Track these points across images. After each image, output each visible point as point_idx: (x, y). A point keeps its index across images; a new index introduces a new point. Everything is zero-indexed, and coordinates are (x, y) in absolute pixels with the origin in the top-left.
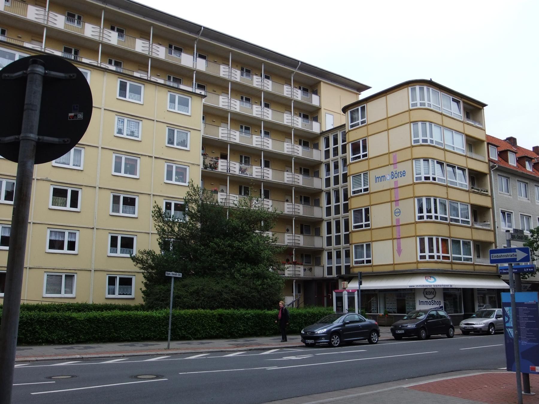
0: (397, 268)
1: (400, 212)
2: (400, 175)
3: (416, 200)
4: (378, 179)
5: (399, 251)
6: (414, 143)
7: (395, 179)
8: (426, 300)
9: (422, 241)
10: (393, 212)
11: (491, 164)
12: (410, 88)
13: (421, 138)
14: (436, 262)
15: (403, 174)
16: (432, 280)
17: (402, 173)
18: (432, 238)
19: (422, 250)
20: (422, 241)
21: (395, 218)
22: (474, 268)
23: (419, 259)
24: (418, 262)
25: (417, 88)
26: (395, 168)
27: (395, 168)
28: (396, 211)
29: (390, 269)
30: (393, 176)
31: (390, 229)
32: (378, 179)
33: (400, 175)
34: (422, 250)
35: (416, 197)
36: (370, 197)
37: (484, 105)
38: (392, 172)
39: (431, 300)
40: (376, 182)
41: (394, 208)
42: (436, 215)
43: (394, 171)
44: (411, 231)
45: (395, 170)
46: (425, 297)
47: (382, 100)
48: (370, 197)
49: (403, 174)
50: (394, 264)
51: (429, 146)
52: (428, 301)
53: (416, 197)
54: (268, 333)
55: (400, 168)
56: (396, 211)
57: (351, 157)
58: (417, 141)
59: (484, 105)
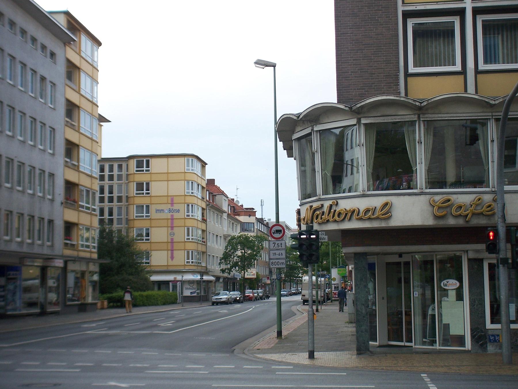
0: (171, 269)
1: (174, 234)
2: (175, 211)
3: (186, 228)
4: (157, 211)
5: (172, 258)
6: (187, 193)
7: (171, 213)
8: (189, 287)
9: (188, 253)
10: (169, 234)
11: (208, 203)
12: (186, 158)
13: (191, 191)
14: (194, 265)
15: (178, 211)
16: (195, 276)
17: (177, 211)
18: (193, 251)
19: (188, 259)
20: (188, 253)
21: (170, 237)
22: (91, 255)
23: (186, 264)
24: (185, 265)
25: (190, 159)
26: (172, 206)
27: (172, 206)
28: (173, 235)
29: (165, 269)
30: (170, 211)
31: (166, 244)
32: (157, 211)
33: (175, 211)
34: (188, 259)
35: (186, 226)
36: (151, 223)
37: (207, 164)
38: (169, 209)
39: (192, 287)
40: (156, 212)
41: (170, 231)
42: (192, 237)
43: (171, 208)
44: (181, 246)
45: (172, 207)
46: (189, 285)
47: (165, 160)
48: (151, 223)
49: (178, 211)
50: (168, 266)
51: (191, 196)
52: (191, 287)
53: (186, 226)
54: (461, 272)
55: (176, 207)
56: (173, 235)
57: (135, 192)
58: (188, 193)
59: (207, 164)
